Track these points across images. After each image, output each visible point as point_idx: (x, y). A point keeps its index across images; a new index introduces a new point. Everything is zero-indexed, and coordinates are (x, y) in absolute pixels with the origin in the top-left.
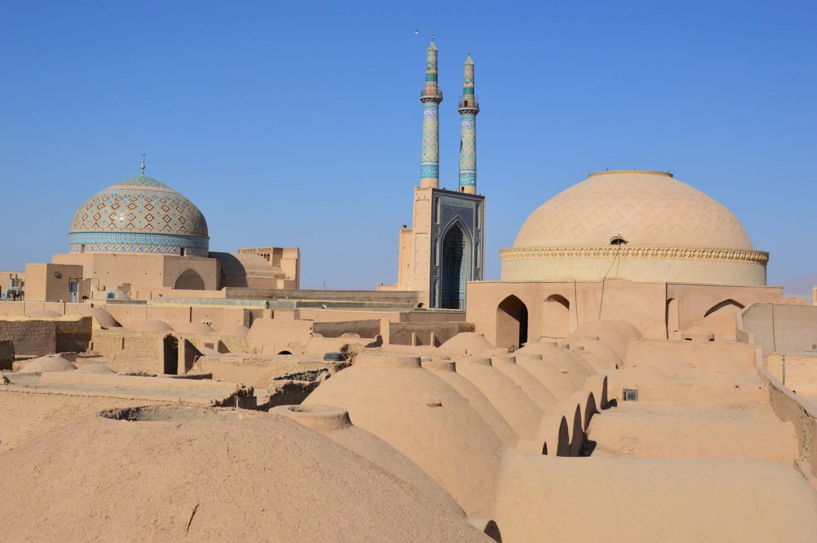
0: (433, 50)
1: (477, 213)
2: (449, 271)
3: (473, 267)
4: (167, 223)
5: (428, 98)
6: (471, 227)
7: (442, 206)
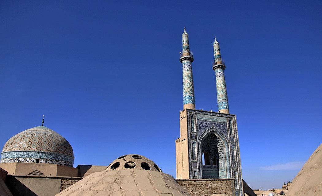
3: (231, 161)
4: (58, 148)
6: (226, 134)
7: (197, 121)
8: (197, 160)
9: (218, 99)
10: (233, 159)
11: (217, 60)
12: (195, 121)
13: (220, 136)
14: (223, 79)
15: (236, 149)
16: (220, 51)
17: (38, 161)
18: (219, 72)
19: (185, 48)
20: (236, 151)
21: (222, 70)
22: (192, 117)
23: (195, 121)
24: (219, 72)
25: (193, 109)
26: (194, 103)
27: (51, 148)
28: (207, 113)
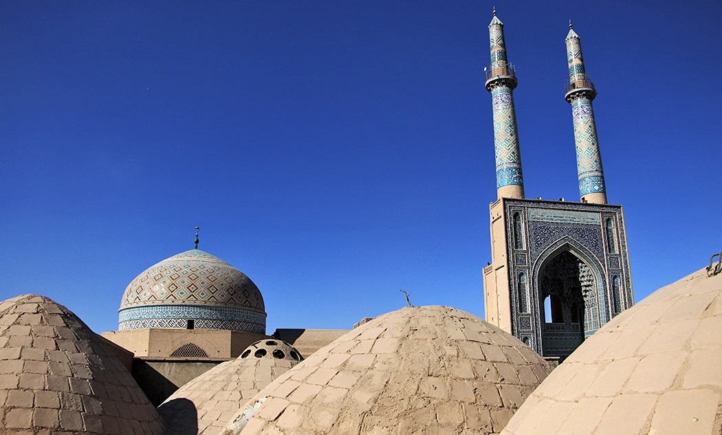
9: (498, 162)
11: (576, 78)
12: (523, 225)
14: (590, 123)
15: (623, 285)
16: (582, 54)
17: (191, 325)
20: (624, 290)
21: (587, 100)
22: (516, 215)
23: (523, 225)
25: (516, 198)
27: (216, 295)
28: (551, 206)
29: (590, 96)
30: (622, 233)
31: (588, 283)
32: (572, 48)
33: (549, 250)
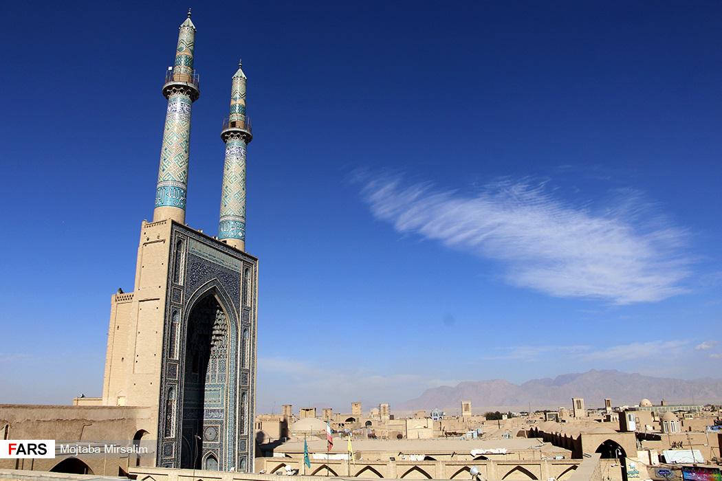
0: (188, 26)
1: (245, 282)
2: (198, 374)
5: (176, 86)
7: (190, 256)
8: (178, 359)
9: (162, 175)
10: (243, 364)
11: (236, 117)
13: (225, 305)
16: (248, 96)
18: (178, 105)
19: (183, 62)
22: (179, 243)
24: (178, 105)
25: (180, 223)
26: (184, 208)
28: (208, 242)
29: (193, 95)
30: (255, 286)
31: (220, 332)
32: (238, 86)
33: (201, 290)
